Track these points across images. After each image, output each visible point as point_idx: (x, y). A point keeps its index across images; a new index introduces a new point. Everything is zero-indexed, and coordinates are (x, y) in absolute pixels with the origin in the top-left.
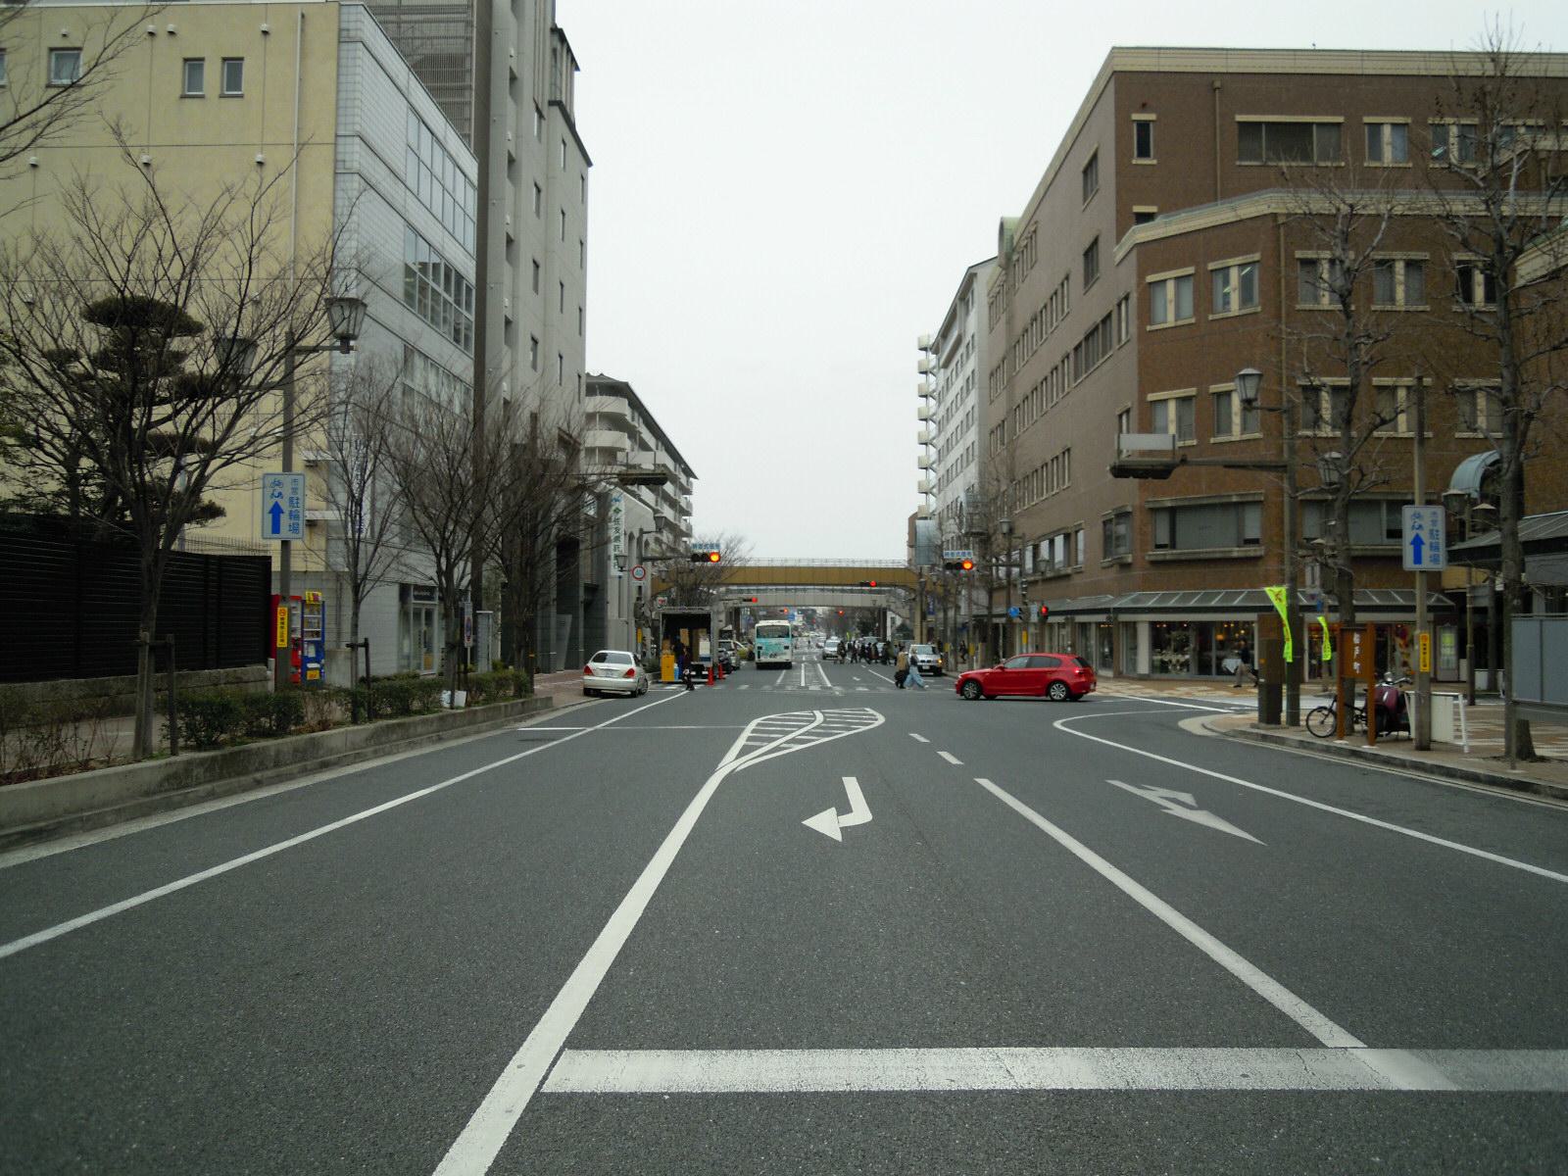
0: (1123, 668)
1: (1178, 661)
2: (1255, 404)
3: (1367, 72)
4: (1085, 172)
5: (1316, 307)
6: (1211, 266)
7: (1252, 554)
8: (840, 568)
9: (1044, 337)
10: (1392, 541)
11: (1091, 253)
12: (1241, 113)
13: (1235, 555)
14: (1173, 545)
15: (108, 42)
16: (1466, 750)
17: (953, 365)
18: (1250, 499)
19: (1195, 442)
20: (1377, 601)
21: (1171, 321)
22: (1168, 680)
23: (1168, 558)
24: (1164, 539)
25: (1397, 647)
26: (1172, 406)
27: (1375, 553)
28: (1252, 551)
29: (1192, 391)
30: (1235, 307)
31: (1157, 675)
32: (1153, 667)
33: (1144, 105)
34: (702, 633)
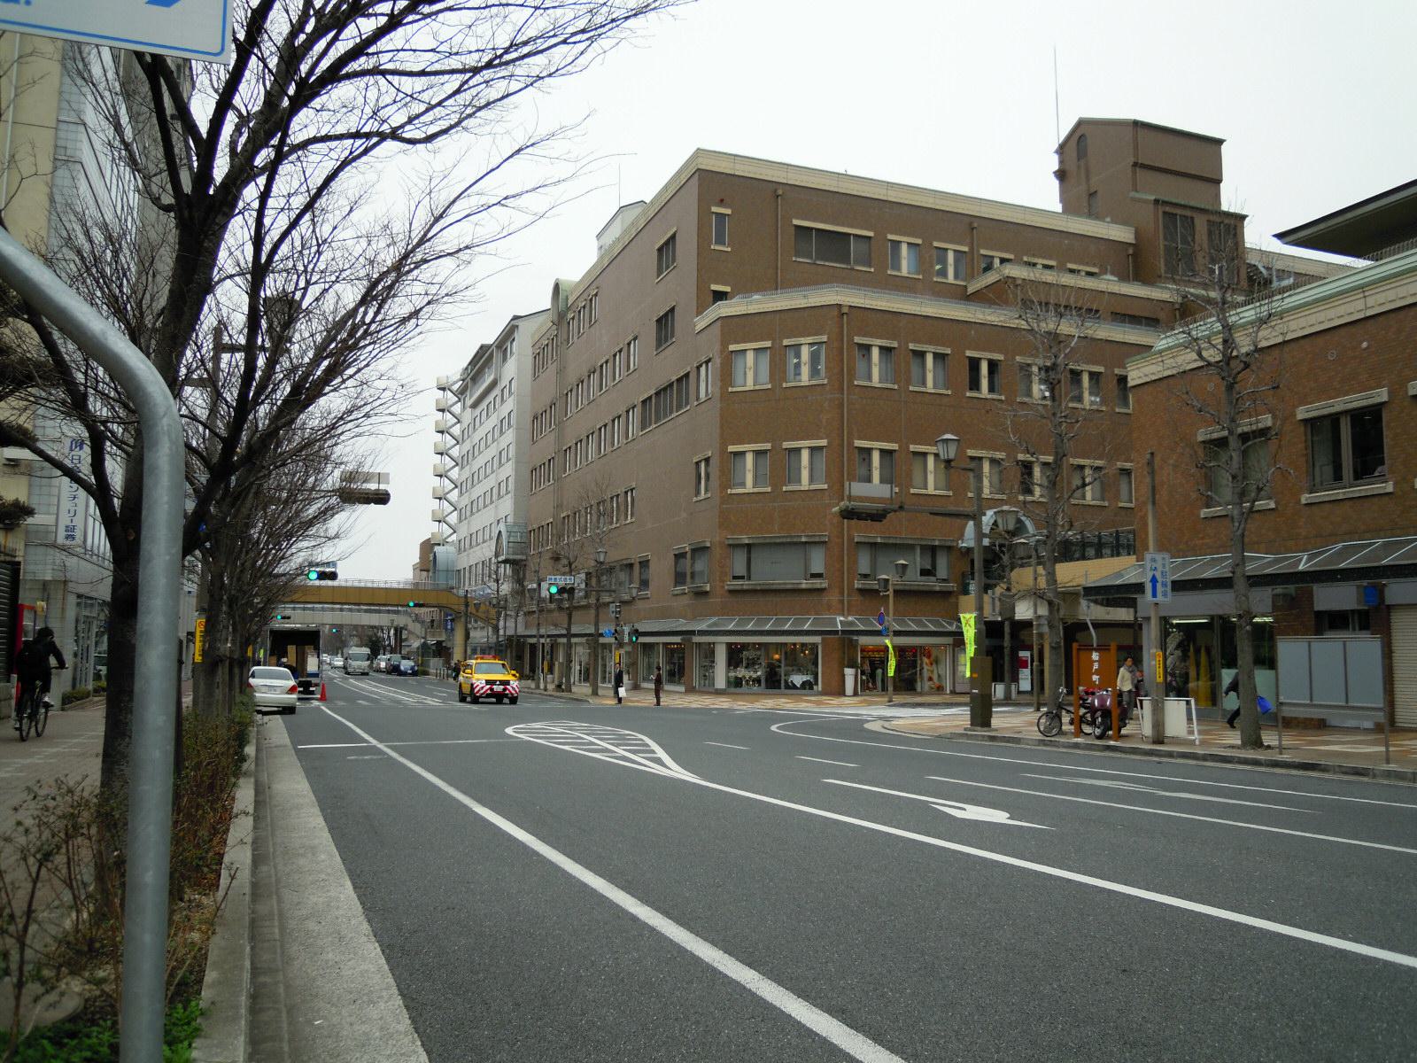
0: (696, 683)
1: (750, 677)
2: (953, 464)
3: (890, 199)
4: (660, 250)
5: (869, 384)
6: (786, 342)
7: (818, 586)
8: (346, 587)
9: (604, 390)
10: (924, 578)
11: (665, 323)
12: (797, 218)
13: (804, 586)
14: (749, 579)
15: (520, 39)
16: (1197, 743)
17: (484, 405)
18: (817, 539)
19: (769, 489)
20: (915, 628)
21: (750, 385)
22: (742, 694)
23: (745, 587)
24: (740, 569)
25: (925, 666)
26: (749, 458)
27: (912, 588)
28: (818, 583)
29: (768, 446)
30: (805, 378)
31: (733, 690)
32: (729, 683)
33: (722, 201)
34: (309, 649)
